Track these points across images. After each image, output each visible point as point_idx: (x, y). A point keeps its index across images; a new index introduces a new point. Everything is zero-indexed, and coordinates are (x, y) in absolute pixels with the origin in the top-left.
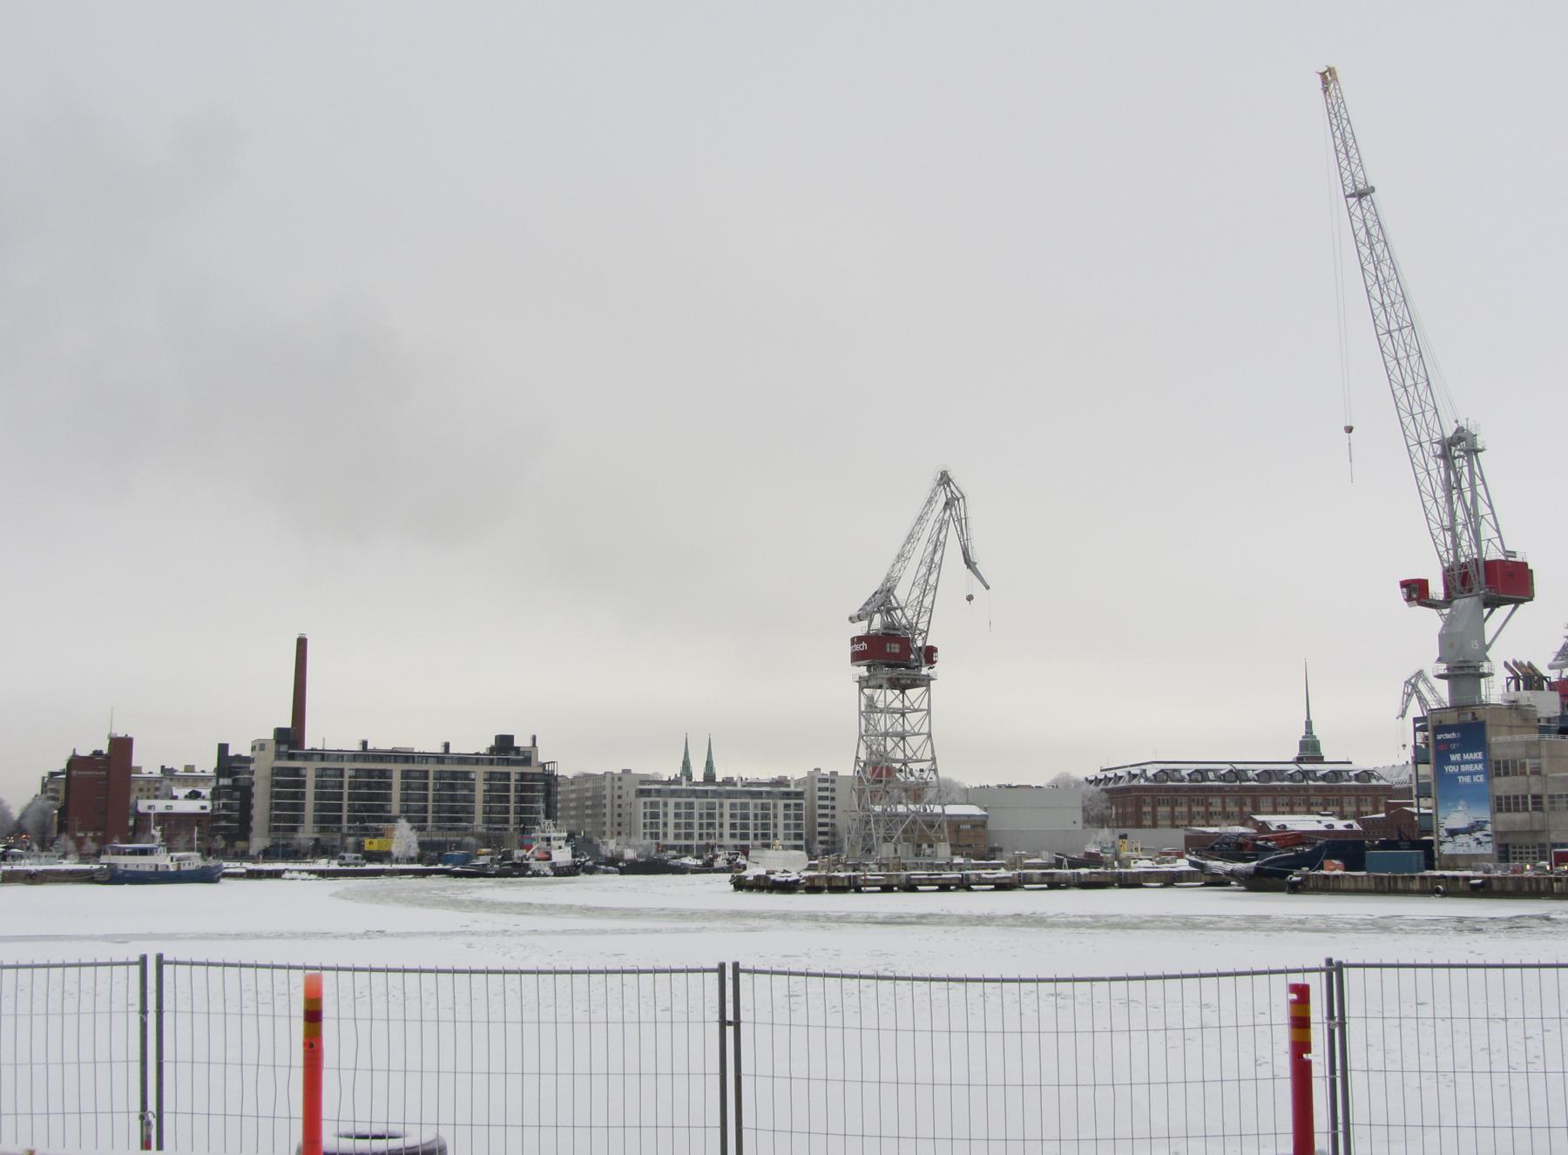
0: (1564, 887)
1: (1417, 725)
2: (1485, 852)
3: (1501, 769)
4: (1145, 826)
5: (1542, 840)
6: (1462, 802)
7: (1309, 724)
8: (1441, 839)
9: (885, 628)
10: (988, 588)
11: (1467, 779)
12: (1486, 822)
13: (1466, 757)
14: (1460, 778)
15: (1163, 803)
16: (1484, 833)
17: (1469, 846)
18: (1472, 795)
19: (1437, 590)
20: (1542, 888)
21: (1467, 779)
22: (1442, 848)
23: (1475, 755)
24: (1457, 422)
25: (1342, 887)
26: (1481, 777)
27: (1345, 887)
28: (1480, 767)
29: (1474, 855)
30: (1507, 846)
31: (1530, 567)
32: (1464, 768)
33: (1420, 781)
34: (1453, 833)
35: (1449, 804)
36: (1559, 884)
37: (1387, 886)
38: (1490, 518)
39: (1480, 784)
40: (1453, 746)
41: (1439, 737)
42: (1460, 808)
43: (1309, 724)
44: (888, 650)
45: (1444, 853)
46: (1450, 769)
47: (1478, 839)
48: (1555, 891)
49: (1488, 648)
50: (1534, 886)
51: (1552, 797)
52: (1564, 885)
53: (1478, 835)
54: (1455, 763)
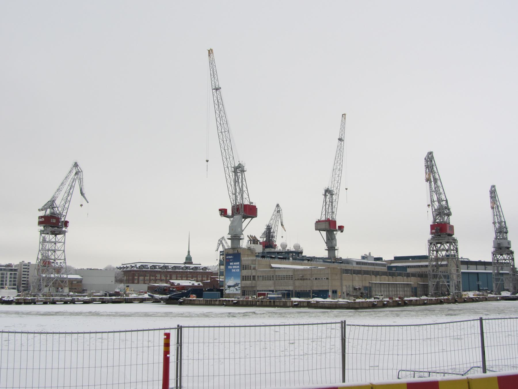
1: (221, 253)
3: (244, 267)
4: (135, 283)
5: (255, 289)
6: (233, 278)
7: (189, 252)
8: (226, 289)
9: (51, 214)
10: (88, 202)
11: (234, 270)
12: (239, 284)
13: (235, 264)
14: (232, 270)
15: (142, 276)
16: (238, 287)
18: (235, 275)
19: (229, 212)
20: (254, 303)
21: (234, 270)
24: (239, 162)
26: (239, 270)
28: (238, 267)
30: (244, 291)
31: (257, 207)
32: (234, 267)
34: (229, 287)
36: (259, 302)
40: (231, 260)
41: (227, 257)
42: (232, 279)
43: (189, 252)
44: (52, 221)
46: (230, 267)
47: (236, 289)
48: (257, 304)
49: (243, 231)
50: (251, 303)
51: (258, 276)
53: (237, 287)
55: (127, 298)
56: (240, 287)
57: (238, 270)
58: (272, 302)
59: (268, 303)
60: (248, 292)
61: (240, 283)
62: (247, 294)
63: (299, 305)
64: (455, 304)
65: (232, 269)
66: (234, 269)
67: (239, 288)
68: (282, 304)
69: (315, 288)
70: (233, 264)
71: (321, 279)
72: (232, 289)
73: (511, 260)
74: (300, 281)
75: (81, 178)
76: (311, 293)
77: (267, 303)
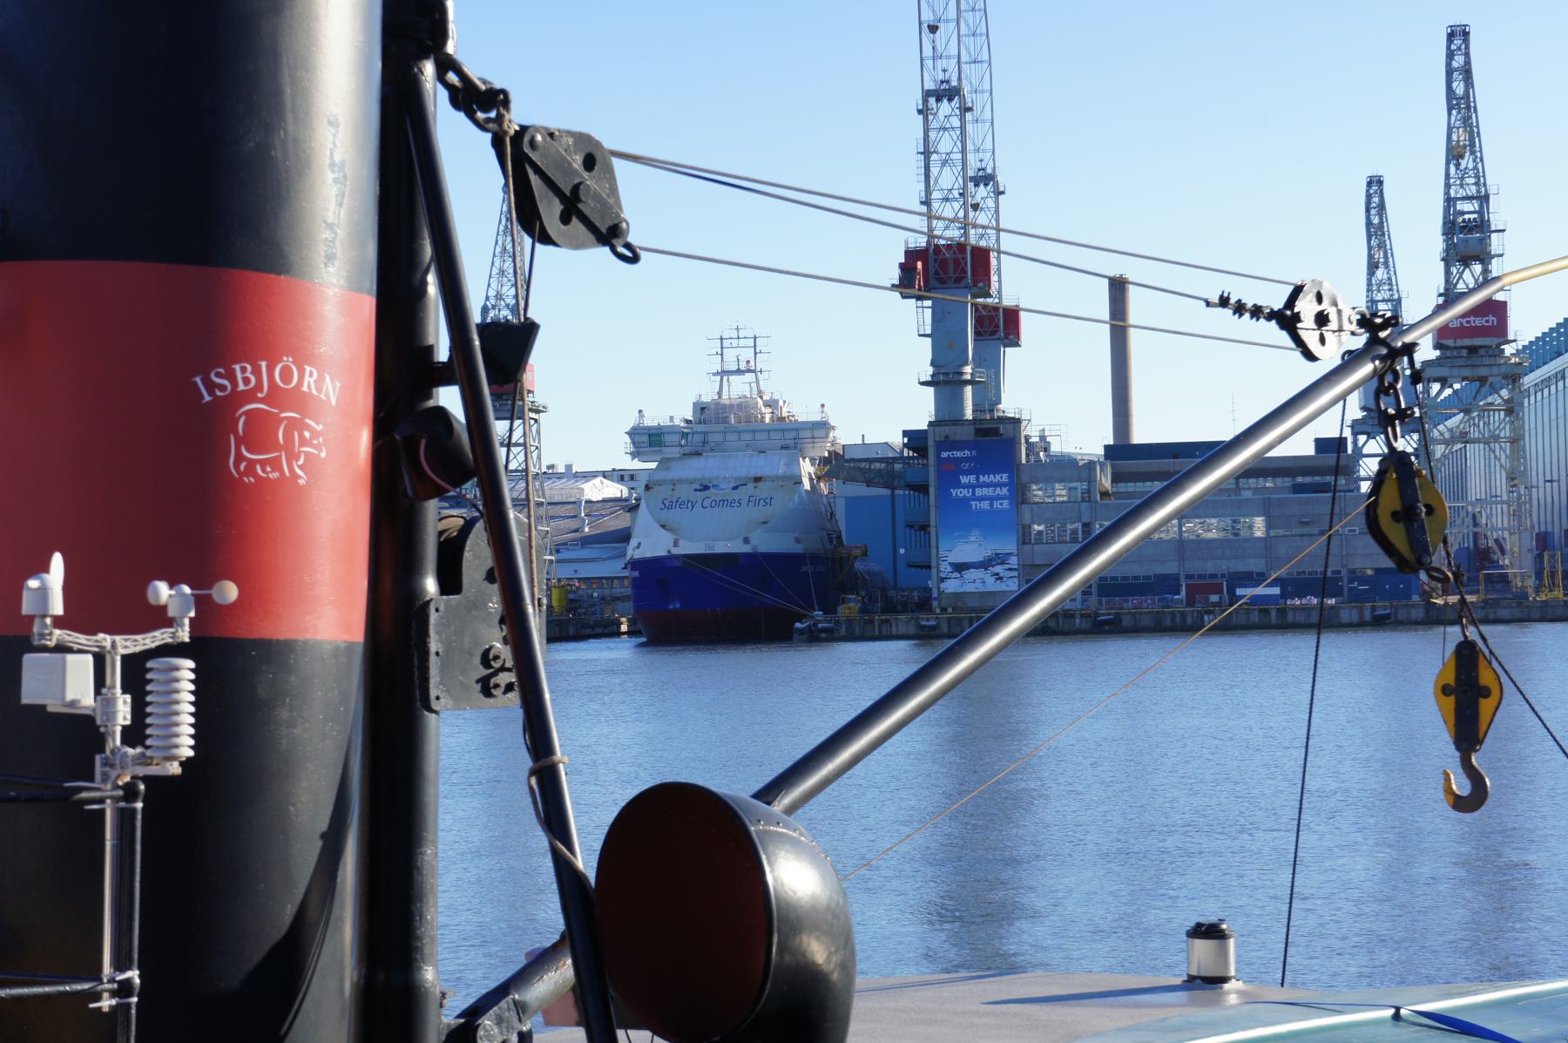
8: (943, 575)
11: (985, 505)
16: (1007, 566)
17: (984, 582)
18: (989, 523)
20: (1189, 621)
21: (985, 505)
22: (943, 586)
23: (998, 477)
25: (894, 632)
27: (900, 633)
28: (1005, 490)
29: (990, 593)
32: (979, 492)
34: (960, 568)
35: (956, 534)
39: (1002, 511)
41: (944, 455)
42: (972, 539)
47: (997, 574)
50: (1178, 619)
53: (998, 569)
54: (968, 486)
56: (1016, 567)
57: (1006, 504)
58: (1273, 614)
59: (1255, 617)
61: (1016, 551)
63: (1393, 619)
64: (489, 86)
65: (974, 500)
66: (982, 499)
67: (1010, 569)
70: (978, 479)
72: (971, 574)
75: (1512, 517)
76: (1345, 580)
77: (1252, 616)
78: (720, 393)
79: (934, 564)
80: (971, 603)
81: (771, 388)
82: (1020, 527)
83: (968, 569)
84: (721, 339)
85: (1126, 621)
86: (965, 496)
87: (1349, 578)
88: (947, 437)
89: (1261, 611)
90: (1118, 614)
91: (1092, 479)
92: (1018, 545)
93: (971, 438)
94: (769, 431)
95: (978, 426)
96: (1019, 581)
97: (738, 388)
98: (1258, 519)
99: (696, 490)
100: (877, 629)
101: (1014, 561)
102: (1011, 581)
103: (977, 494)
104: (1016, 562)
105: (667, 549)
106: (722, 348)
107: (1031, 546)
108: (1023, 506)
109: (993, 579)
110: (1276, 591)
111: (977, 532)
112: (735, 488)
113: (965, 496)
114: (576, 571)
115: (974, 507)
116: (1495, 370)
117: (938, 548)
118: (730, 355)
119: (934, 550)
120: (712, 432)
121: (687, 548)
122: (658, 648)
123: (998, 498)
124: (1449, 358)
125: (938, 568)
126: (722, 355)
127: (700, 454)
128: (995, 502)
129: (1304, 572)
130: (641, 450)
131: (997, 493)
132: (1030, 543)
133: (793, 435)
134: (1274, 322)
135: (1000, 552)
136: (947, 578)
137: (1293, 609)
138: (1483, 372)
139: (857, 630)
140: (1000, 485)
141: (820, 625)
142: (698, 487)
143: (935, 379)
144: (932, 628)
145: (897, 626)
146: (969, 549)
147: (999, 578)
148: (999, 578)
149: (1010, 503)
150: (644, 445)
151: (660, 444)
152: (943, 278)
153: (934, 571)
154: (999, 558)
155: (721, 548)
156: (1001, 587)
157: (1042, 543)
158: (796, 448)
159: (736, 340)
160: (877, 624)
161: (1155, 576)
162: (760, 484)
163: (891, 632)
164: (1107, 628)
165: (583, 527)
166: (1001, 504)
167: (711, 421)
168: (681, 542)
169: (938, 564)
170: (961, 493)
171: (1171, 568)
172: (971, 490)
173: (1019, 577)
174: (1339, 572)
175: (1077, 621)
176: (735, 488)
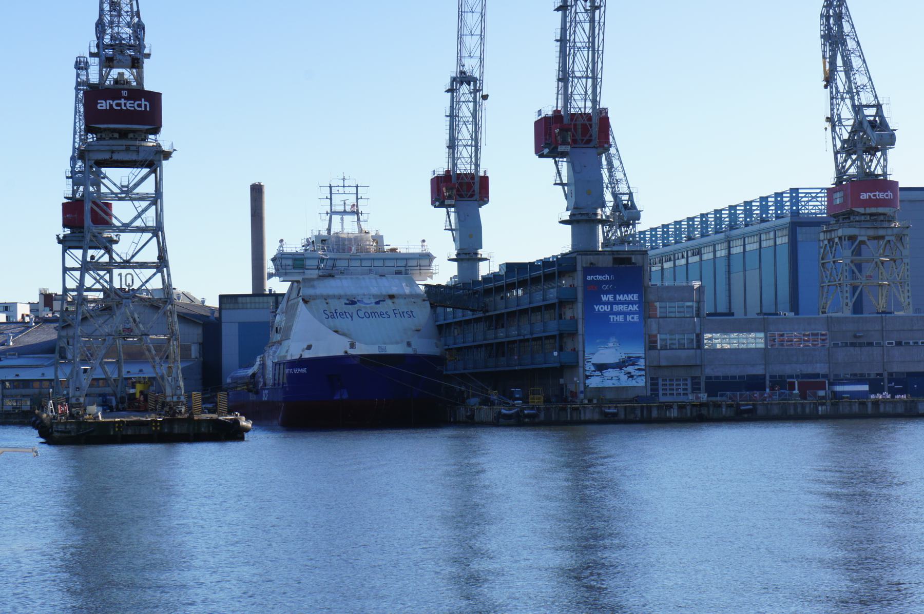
0: (828, 410)
2: (636, 385)
5: (697, 373)
6: (613, 340)
8: (588, 374)
11: (620, 318)
12: (639, 357)
14: (611, 317)
16: (636, 367)
17: (619, 379)
18: (624, 333)
20: (807, 410)
21: (620, 318)
22: (588, 382)
23: (630, 297)
25: (583, 418)
26: (636, 317)
27: (587, 418)
28: (635, 307)
29: (623, 387)
32: (616, 308)
33: (695, 347)
34: (601, 368)
35: (598, 341)
36: (824, 407)
37: (639, 415)
38: (587, 26)
39: (634, 324)
40: (605, 287)
41: (589, 278)
42: (611, 345)
45: (590, 386)
47: (629, 373)
48: (820, 413)
50: (799, 410)
52: (828, 408)
53: (630, 369)
54: (607, 303)
55: (127, 421)
56: (644, 368)
60: (668, 383)
61: (643, 356)
62: (668, 392)
68: (900, 409)
69: (896, 368)
70: (615, 298)
71: (915, 343)
73: (80, 295)
74: (852, 349)
76: (886, 381)
77: (854, 407)
78: (329, 230)
79: (581, 364)
80: (609, 396)
81: (372, 225)
82: (647, 337)
83: (607, 368)
84: (331, 187)
85: (761, 411)
86: (605, 311)
87: (888, 379)
88: (591, 264)
89: (860, 403)
90: (753, 405)
91: (701, 300)
92: (645, 350)
93: (610, 264)
94: (373, 259)
95: (615, 256)
96: (646, 378)
97: (347, 227)
98: (613, 379)
99: (346, 304)
100: (569, 416)
101: (642, 363)
102: (640, 378)
103: (614, 310)
104: (644, 364)
105: (344, 350)
106: (331, 193)
107: (657, 351)
108: (649, 320)
109: (626, 377)
110: (866, 388)
111: (614, 340)
112: (377, 303)
113: (605, 311)
114: (43, 374)
115: (612, 320)
116: (889, 232)
117: (584, 351)
118: (337, 200)
119: (581, 353)
120: (340, 259)
121: (362, 349)
122: (315, 433)
123: (631, 313)
124: (858, 221)
125: (584, 367)
126: (331, 199)
127: (333, 276)
128: (628, 316)
129: (856, 375)
130: (288, 271)
131: (629, 309)
132: (657, 349)
133: (403, 263)
134: (61, 246)
135: (631, 355)
136: (591, 376)
137: (883, 402)
138: (881, 232)
139: (553, 415)
140: (632, 303)
141: (526, 412)
142: (347, 302)
143: (574, 218)
144: (614, 415)
145: (585, 414)
146: (608, 353)
147: (630, 376)
148: (630, 376)
149: (639, 318)
150: (290, 267)
151: (303, 267)
152: (587, 140)
153: (581, 370)
154: (631, 360)
155: (393, 349)
156: (632, 383)
157: (667, 349)
158: (407, 274)
159: (342, 188)
160: (569, 411)
161: (748, 376)
162: (396, 300)
163: (580, 417)
164: (746, 416)
165: (7, 341)
166: (633, 318)
167: (333, 250)
168: (357, 345)
169: (584, 365)
170: (602, 308)
171: (759, 370)
172: (609, 306)
173: (646, 375)
174: (881, 375)
175: (724, 410)
176: (377, 303)
